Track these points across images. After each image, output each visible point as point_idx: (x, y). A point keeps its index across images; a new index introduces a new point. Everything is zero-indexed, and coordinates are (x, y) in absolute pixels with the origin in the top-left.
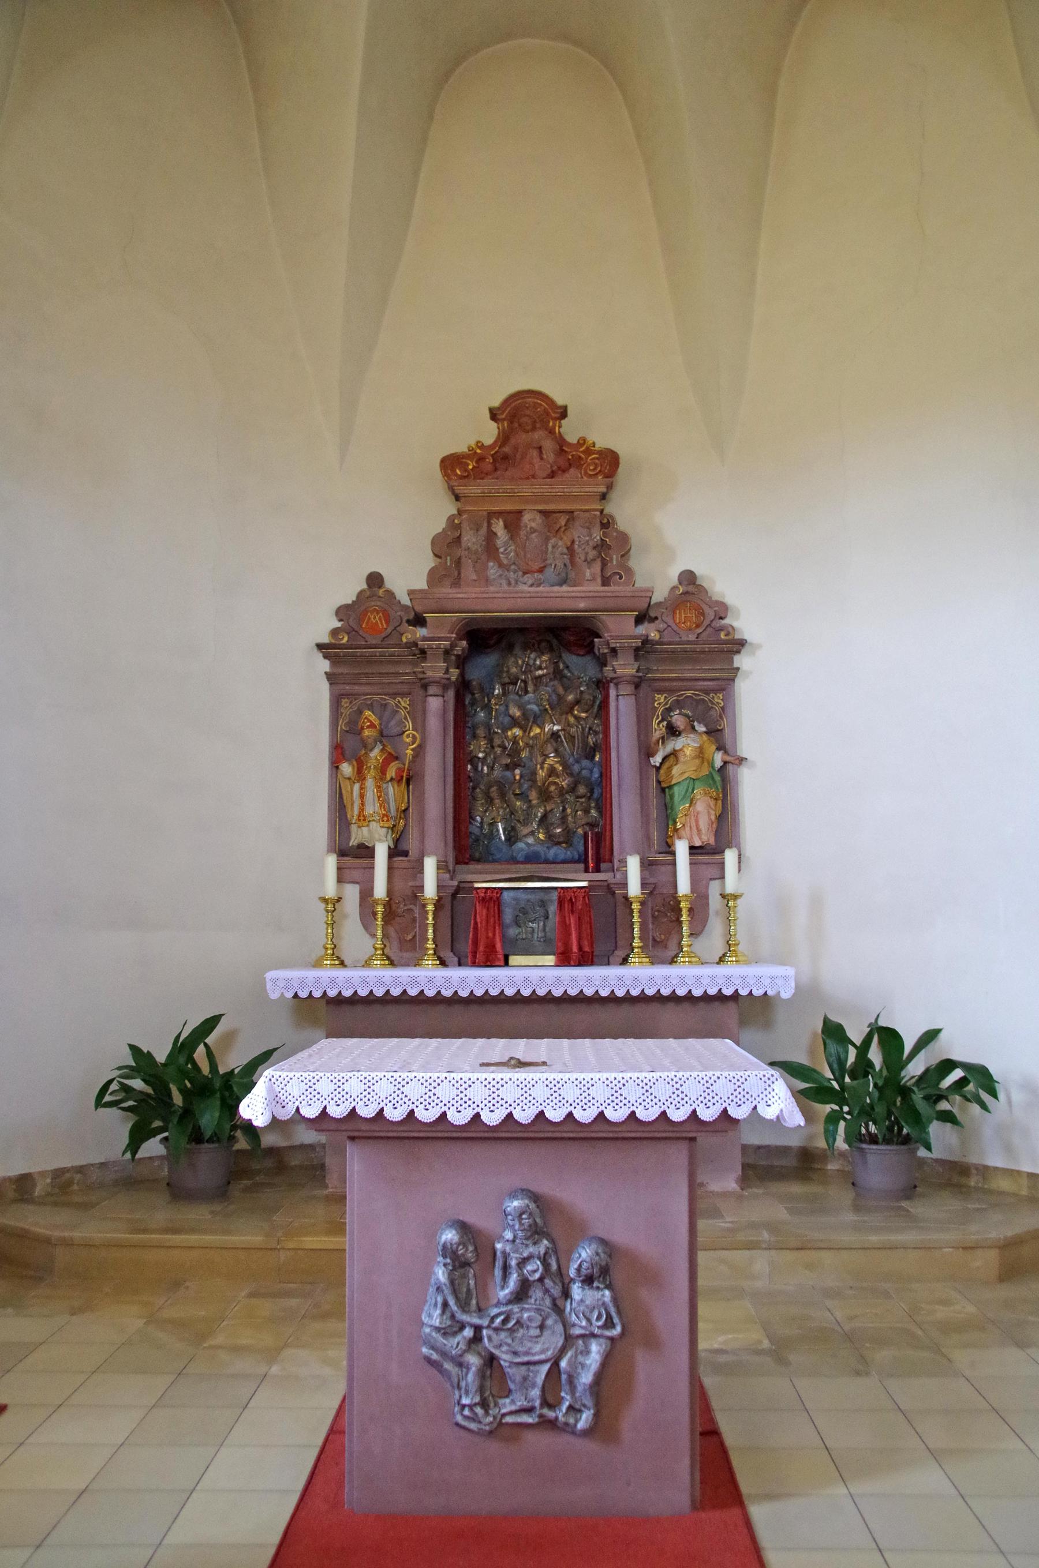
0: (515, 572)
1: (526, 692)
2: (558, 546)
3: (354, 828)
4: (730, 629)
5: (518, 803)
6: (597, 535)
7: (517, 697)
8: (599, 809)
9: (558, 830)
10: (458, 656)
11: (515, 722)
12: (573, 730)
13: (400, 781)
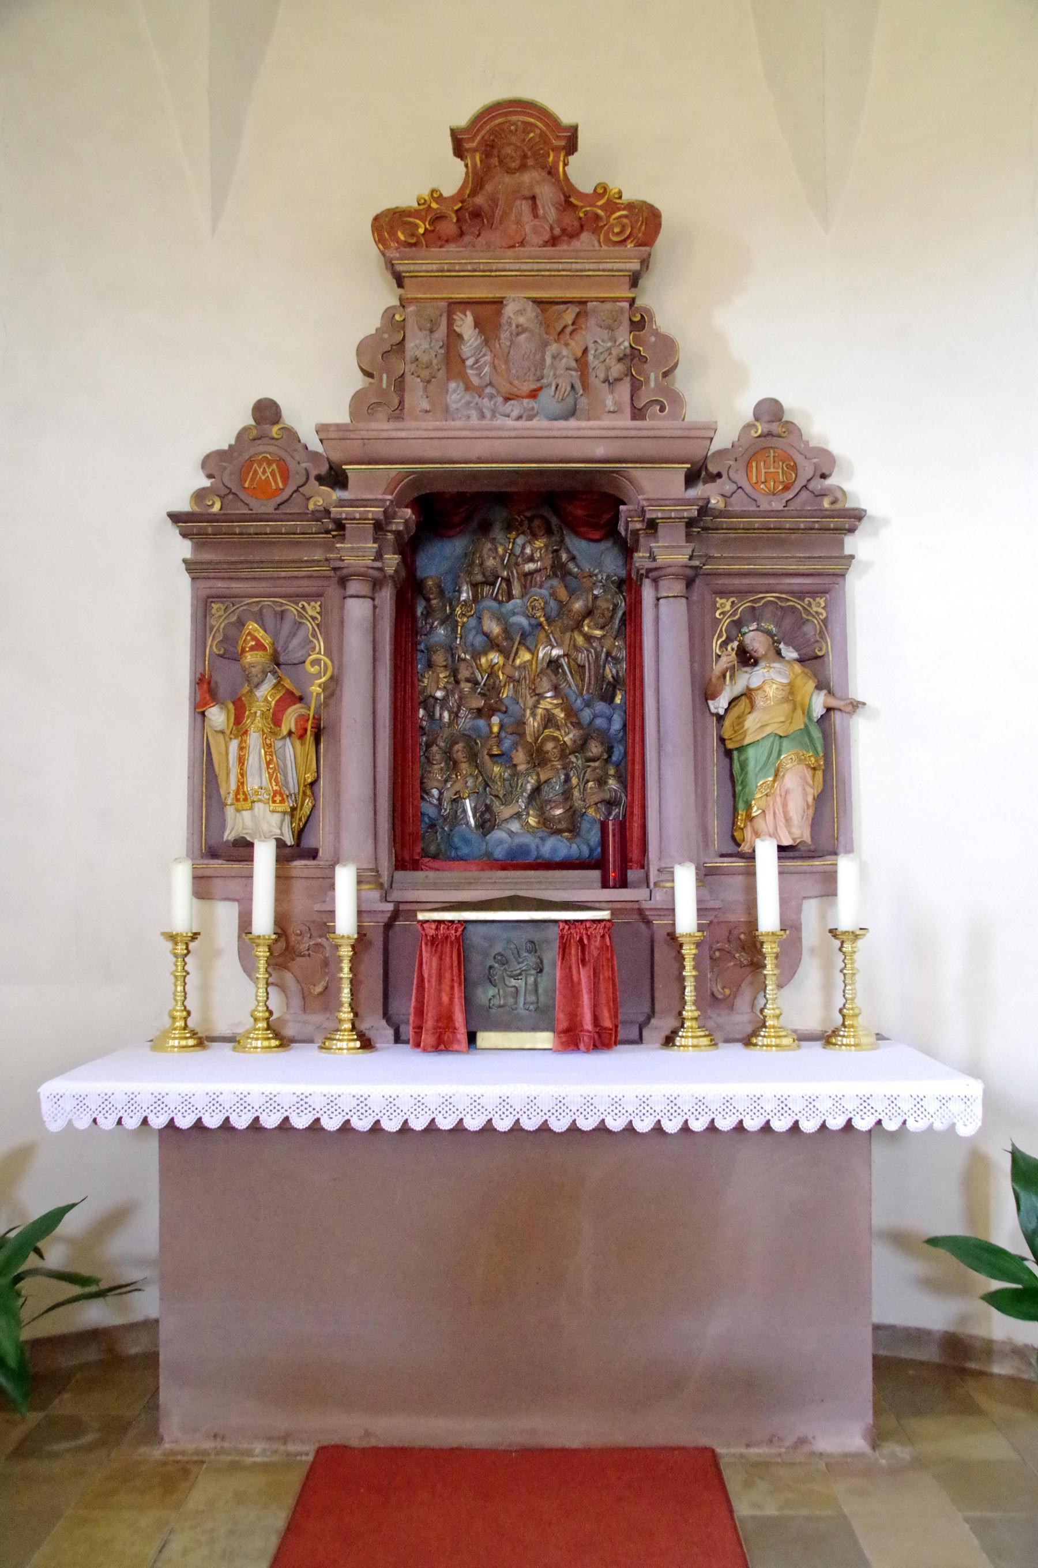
0: (491, 397)
1: (510, 597)
2: (560, 358)
3: (230, 811)
4: (839, 495)
5: (496, 769)
6: (624, 340)
7: (495, 604)
8: (620, 778)
9: (559, 812)
10: (398, 534)
11: (492, 644)
12: (581, 657)
13: (301, 737)
